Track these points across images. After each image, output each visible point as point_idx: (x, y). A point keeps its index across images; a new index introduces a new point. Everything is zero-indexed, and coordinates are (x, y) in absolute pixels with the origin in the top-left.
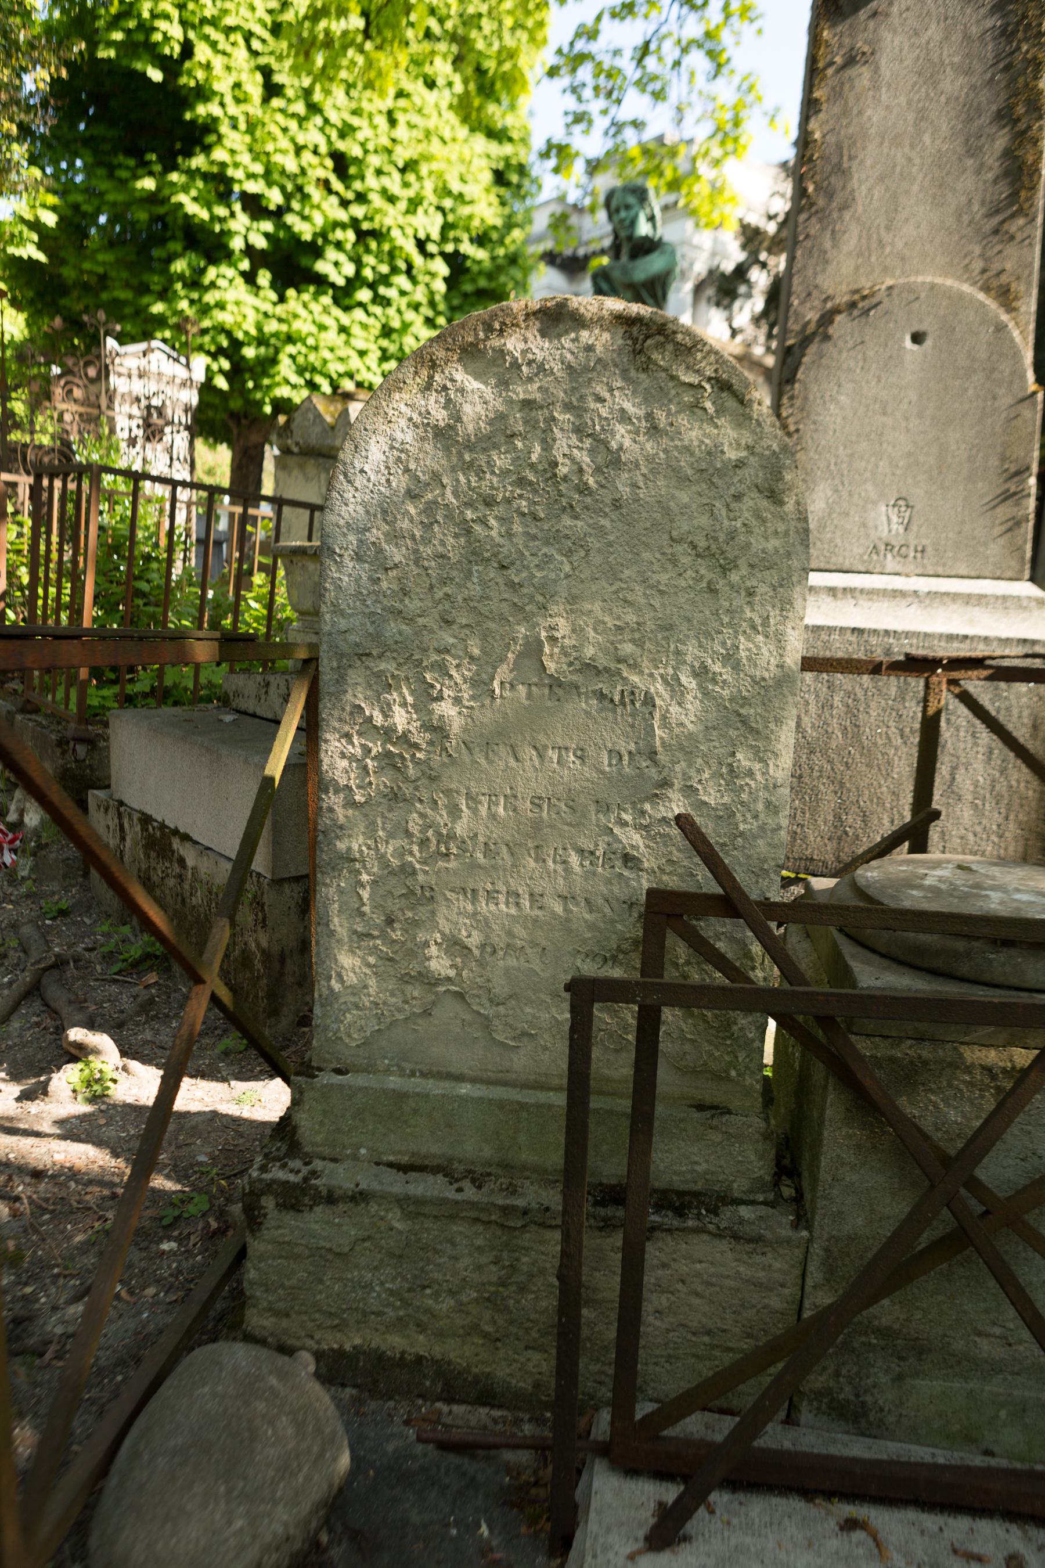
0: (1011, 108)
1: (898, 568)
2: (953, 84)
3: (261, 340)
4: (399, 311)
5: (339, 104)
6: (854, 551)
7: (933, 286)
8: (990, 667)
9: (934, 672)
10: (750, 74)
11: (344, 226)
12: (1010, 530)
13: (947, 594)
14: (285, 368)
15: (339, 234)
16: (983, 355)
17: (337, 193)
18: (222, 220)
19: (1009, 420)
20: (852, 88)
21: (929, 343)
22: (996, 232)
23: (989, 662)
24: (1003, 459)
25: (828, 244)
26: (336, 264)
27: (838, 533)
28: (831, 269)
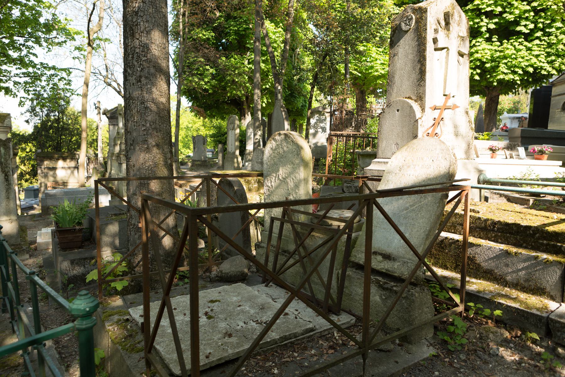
0: (420, 59)
2: (411, 57)
3: (493, 60)
4: (556, 36)
14: (503, 68)
18: (478, 23)
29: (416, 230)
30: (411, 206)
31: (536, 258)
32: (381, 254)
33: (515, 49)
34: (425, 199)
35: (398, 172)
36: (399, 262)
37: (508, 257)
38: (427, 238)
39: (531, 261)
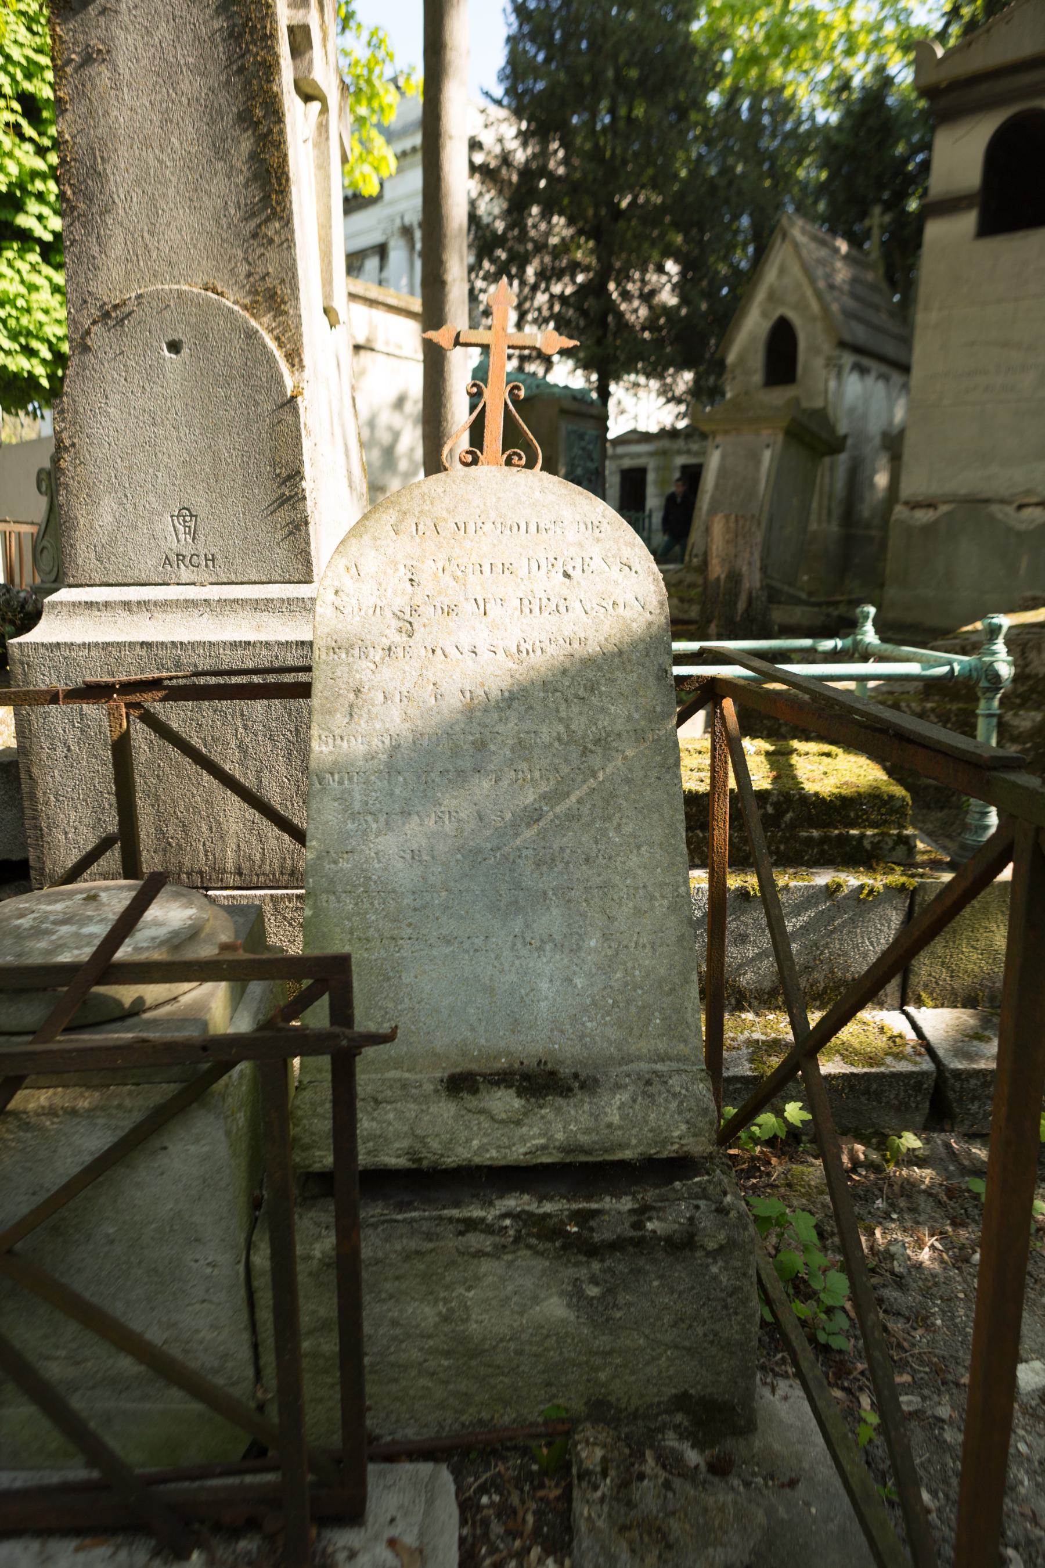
1: (193, 578)
5: (21, 40)
6: (148, 564)
7: (180, 293)
8: (168, 687)
9: (111, 697)
10: (377, 29)
11: (43, 176)
12: (291, 533)
13: (236, 601)
15: (39, 185)
16: (239, 362)
17: (31, 140)
19: (272, 426)
20: (94, 87)
21: (185, 351)
22: (255, 236)
23: (166, 683)
24: (274, 465)
25: (95, 250)
26: (40, 218)
27: (130, 546)
28: (102, 275)
29: (628, 908)
30: (553, 797)
31: (831, 891)
32: (503, 1079)
33: (22, 282)
34: (607, 758)
35: (400, 639)
36: (618, 1087)
37: (744, 912)
38: (183, 895)
39: (816, 904)
